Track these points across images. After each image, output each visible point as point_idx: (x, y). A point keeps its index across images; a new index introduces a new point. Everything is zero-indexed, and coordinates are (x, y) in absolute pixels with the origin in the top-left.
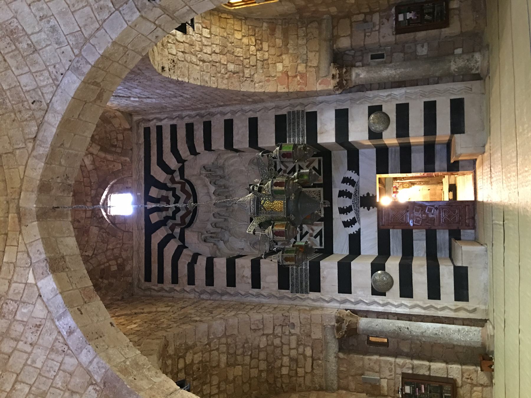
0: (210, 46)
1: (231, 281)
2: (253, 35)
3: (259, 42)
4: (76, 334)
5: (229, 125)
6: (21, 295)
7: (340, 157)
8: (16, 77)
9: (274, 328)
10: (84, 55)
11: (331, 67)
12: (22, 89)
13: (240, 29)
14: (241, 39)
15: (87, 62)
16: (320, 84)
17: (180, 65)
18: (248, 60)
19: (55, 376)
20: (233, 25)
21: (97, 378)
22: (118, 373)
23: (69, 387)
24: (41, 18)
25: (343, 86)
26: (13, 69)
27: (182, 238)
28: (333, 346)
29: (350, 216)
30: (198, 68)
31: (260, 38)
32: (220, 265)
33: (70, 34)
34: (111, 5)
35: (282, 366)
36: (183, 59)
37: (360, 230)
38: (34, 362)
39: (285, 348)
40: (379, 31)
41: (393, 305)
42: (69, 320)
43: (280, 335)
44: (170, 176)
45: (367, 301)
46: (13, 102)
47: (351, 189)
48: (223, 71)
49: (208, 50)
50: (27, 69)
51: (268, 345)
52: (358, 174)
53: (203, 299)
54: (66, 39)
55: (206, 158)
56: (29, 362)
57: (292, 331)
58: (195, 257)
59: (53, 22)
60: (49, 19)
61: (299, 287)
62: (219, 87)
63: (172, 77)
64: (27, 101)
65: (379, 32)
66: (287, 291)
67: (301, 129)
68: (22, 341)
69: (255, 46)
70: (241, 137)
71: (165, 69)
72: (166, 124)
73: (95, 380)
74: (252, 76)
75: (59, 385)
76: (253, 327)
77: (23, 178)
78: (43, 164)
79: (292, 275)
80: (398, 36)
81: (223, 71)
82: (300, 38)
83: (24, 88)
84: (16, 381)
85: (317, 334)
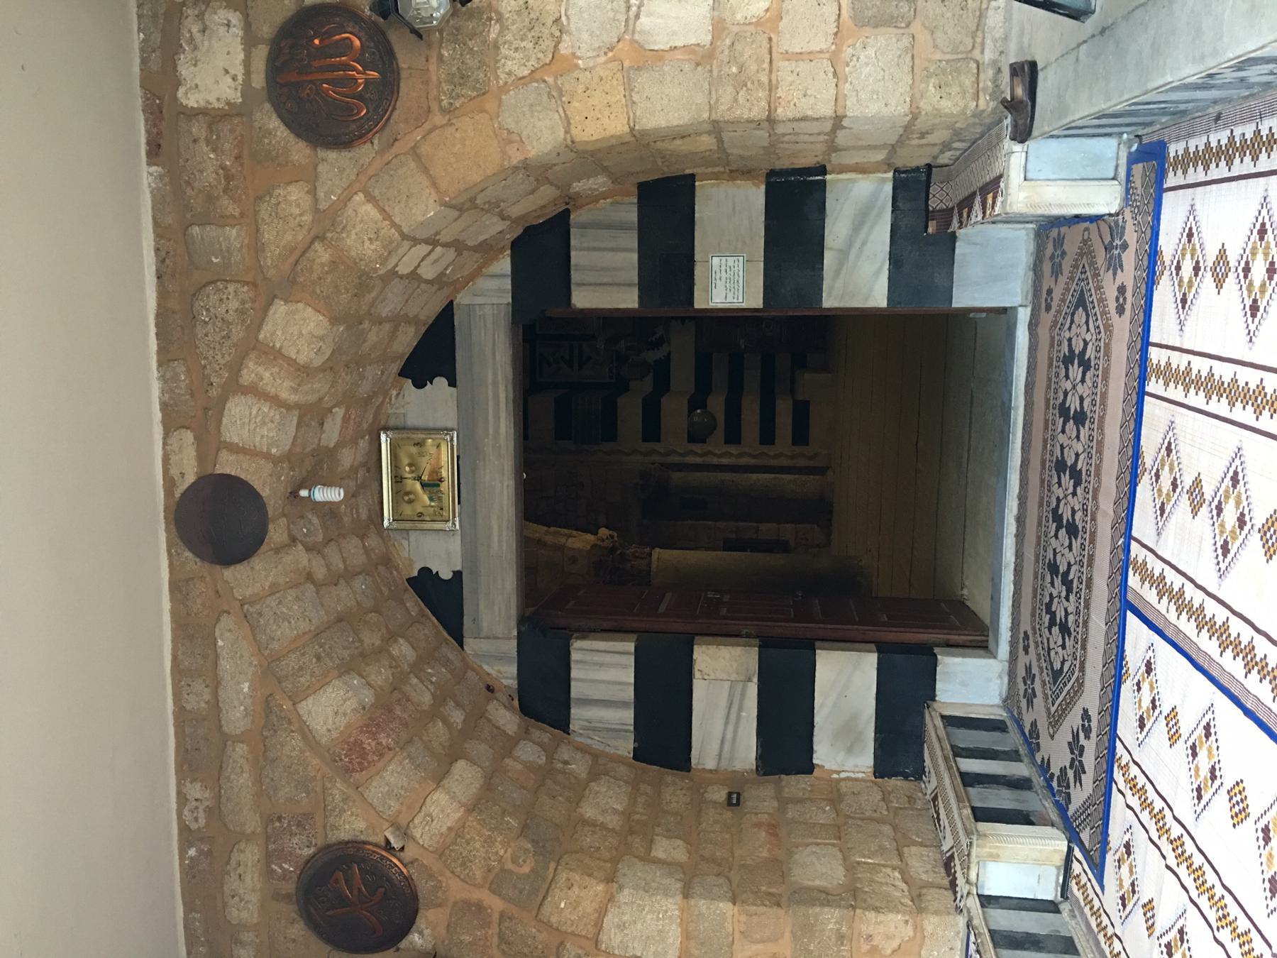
37: (669, 354)
41: (715, 455)
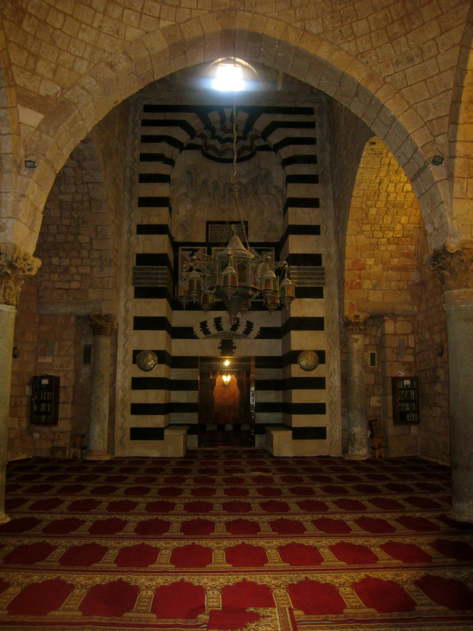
0: (395, 191)
1: (145, 202)
2: (403, 235)
3: (396, 241)
4: (110, 71)
5: (313, 203)
6: (148, 13)
7: (275, 320)
8: (367, 17)
9: (98, 250)
10: (384, 87)
11: (366, 314)
12: (354, 22)
13: (410, 222)
14: (400, 222)
15: (378, 90)
16: (350, 303)
17: (377, 160)
18: (378, 229)
19: (70, 53)
20: (415, 215)
21: (68, 95)
22: (73, 115)
23: (60, 68)
24: (421, 50)
25: (347, 325)
26: (374, 15)
27: (191, 147)
28: (83, 311)
29: (212, 329)
30: (373, 178)
31: (400, 242)
32: (161, 190)
33: (405, 75)
34: (430, 118)
35: (61, 258)
36: (382, 163)
37: (197, 338)
38: (84, 30)
39: (78, 262)
40: (397, 361)
41: (124, 371)
42: (124, 64)
43: (91, 256)
44: (260, 135)
45: (126, 345)
46: (341, 12)
47: (241, 330)
48: (369, 203)
49: (391, 188)
50: (373, 28)
51: (81, 244)
52: (256, 338)
53: (125, 171)
54: (401, 71)
55: (278, 175)
56: (83, 26)
57: (96, 269)
58: (170, 162)
59: (417, 60)
60: (420, 56)
61: (139, 276)
62: (352, 198)
63: (364, 152)
64: (342, 26)
65: (395, 361)
66: (135, 264)
67: (305, 281)
68: (104, 18)
69: (393, 237)
70: (300, 216)
71: (373, 146)
72: (316, 133)
73: (66, 92)
74: (362, 232)
75: (62, 57)
76: (99, 229)
77: (266, 16)
78: (279, 38)
79: (152, 269)
80: (390, 379)
81: (369, 203)
82: (397, 283)
83: (355, 24)
84: (65, 14)
85: (93, 294)
